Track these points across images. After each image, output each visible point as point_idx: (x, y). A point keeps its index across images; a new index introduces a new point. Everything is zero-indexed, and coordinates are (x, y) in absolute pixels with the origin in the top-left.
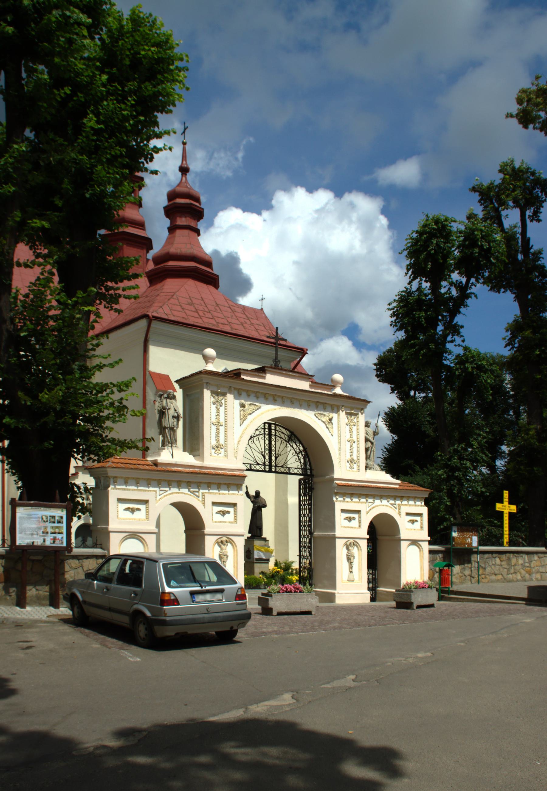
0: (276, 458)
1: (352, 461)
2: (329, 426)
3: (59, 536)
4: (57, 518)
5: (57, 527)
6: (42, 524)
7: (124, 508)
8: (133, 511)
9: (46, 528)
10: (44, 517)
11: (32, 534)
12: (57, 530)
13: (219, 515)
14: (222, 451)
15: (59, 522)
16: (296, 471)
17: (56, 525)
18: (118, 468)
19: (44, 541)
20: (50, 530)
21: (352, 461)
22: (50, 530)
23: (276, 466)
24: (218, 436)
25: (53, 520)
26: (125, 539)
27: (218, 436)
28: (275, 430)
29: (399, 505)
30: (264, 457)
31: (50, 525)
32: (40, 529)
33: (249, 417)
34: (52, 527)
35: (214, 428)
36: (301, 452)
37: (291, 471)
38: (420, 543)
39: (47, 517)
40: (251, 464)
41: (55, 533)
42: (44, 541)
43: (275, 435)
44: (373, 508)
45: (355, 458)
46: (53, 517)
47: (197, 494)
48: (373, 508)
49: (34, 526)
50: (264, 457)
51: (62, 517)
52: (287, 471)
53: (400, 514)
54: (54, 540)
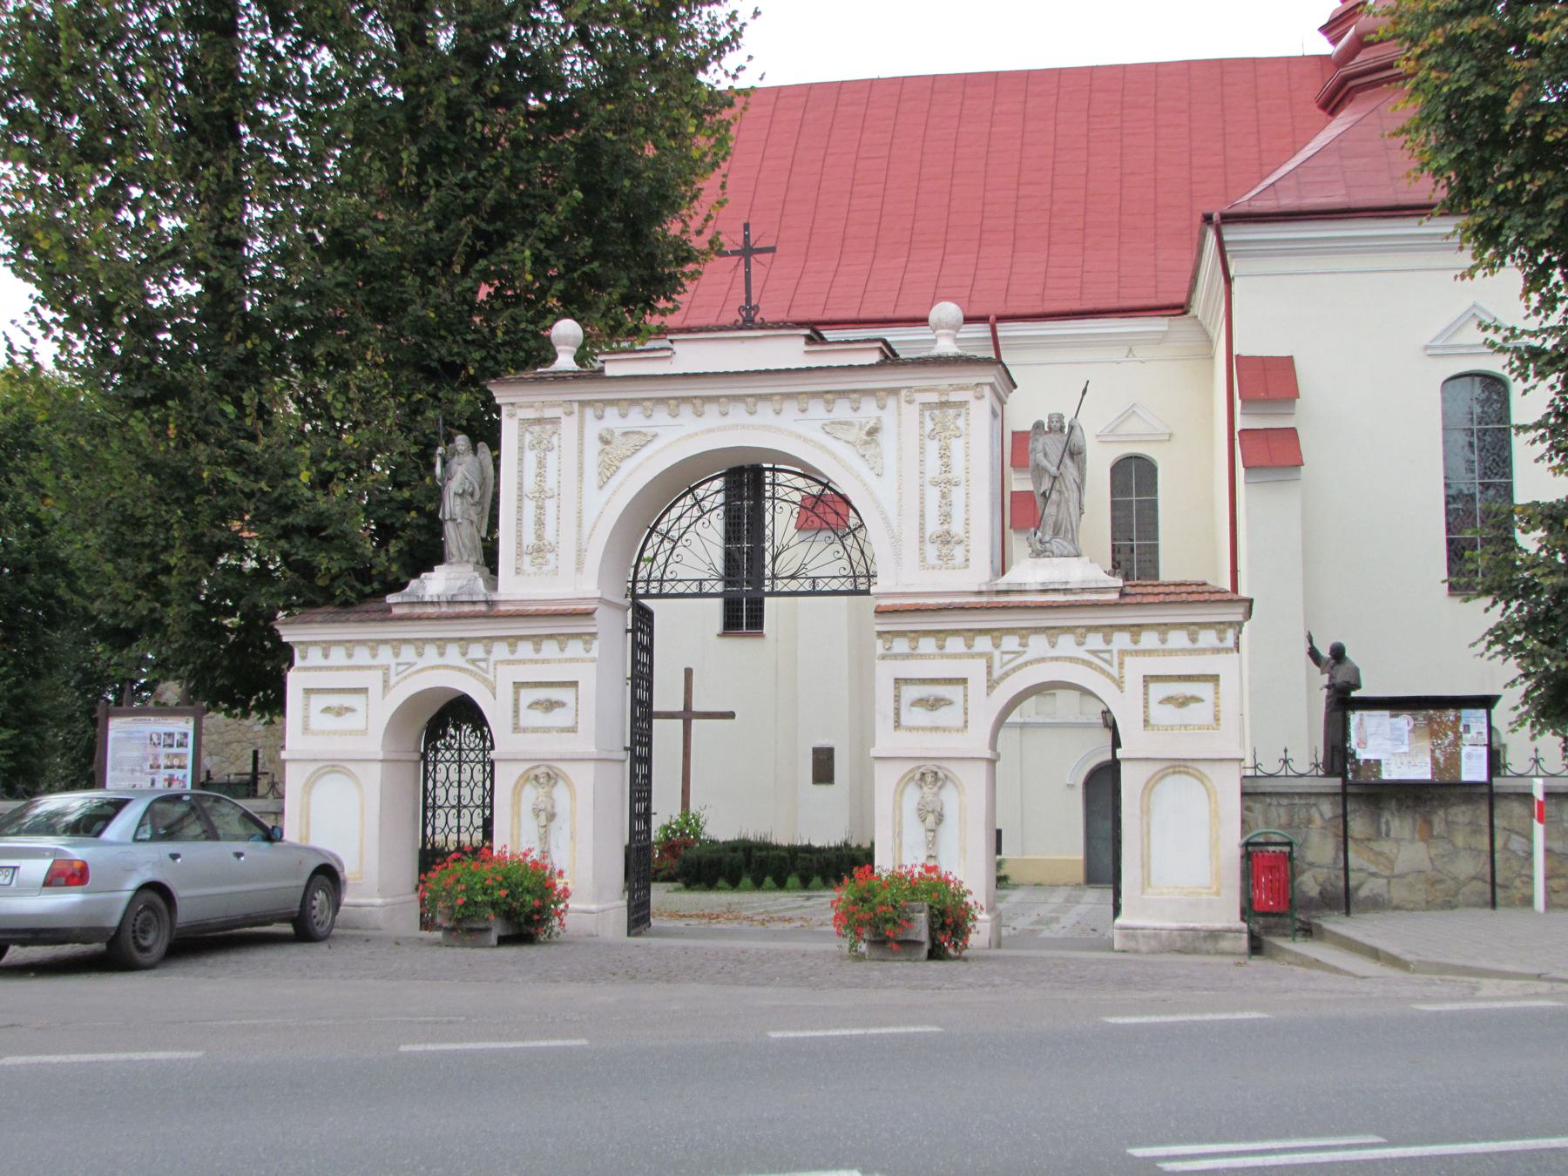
0: (774, 559)
1: (945, 539)
2: (870, 451)
3: (179, 773)
4: (177, 737)
5: (176, 755)
6: (151, 749)
7: (1161, 697)
8: (341, 711)
9: (156, 757)
10: (155, 737)
11: (133, 771)
12: (176, 762)
13: (1170, 707)
14: (550, 556)
15: (181, 745)
16: (835, 585)
17: (175, 750)
18: (419, 618)
19: (153, 783)
20: (163, 761)
21: (945, 539)
22: (163, 761)
23: (774, 577)
24: (540, 523)
25: (169, 741)
26: (1160, 776)
27: (540, 523)
28: (773, 484)
29: (1123, 653)
30: (793, 577)
31: (163, 751)
32: (146, 759)
33: (627, 466)
34: (168, 756)
35: (957, 472)
36: (665, 536)
37: (820, 586)
38: (1203, 767)
39: (159, 736)
40: (701, 581)
41: (171, 767)
42: (153, 783)
43: (773, 498)
44: (1019, 667)
45: (957, 528)
46: (171, 735)
47: (483, 665)
48: (1019, 667)
49: (136, 754)
50: (793, 577)
51: (186, 735)
52: (807, 586)
53: (1119, 683)
54: (170, 781)
